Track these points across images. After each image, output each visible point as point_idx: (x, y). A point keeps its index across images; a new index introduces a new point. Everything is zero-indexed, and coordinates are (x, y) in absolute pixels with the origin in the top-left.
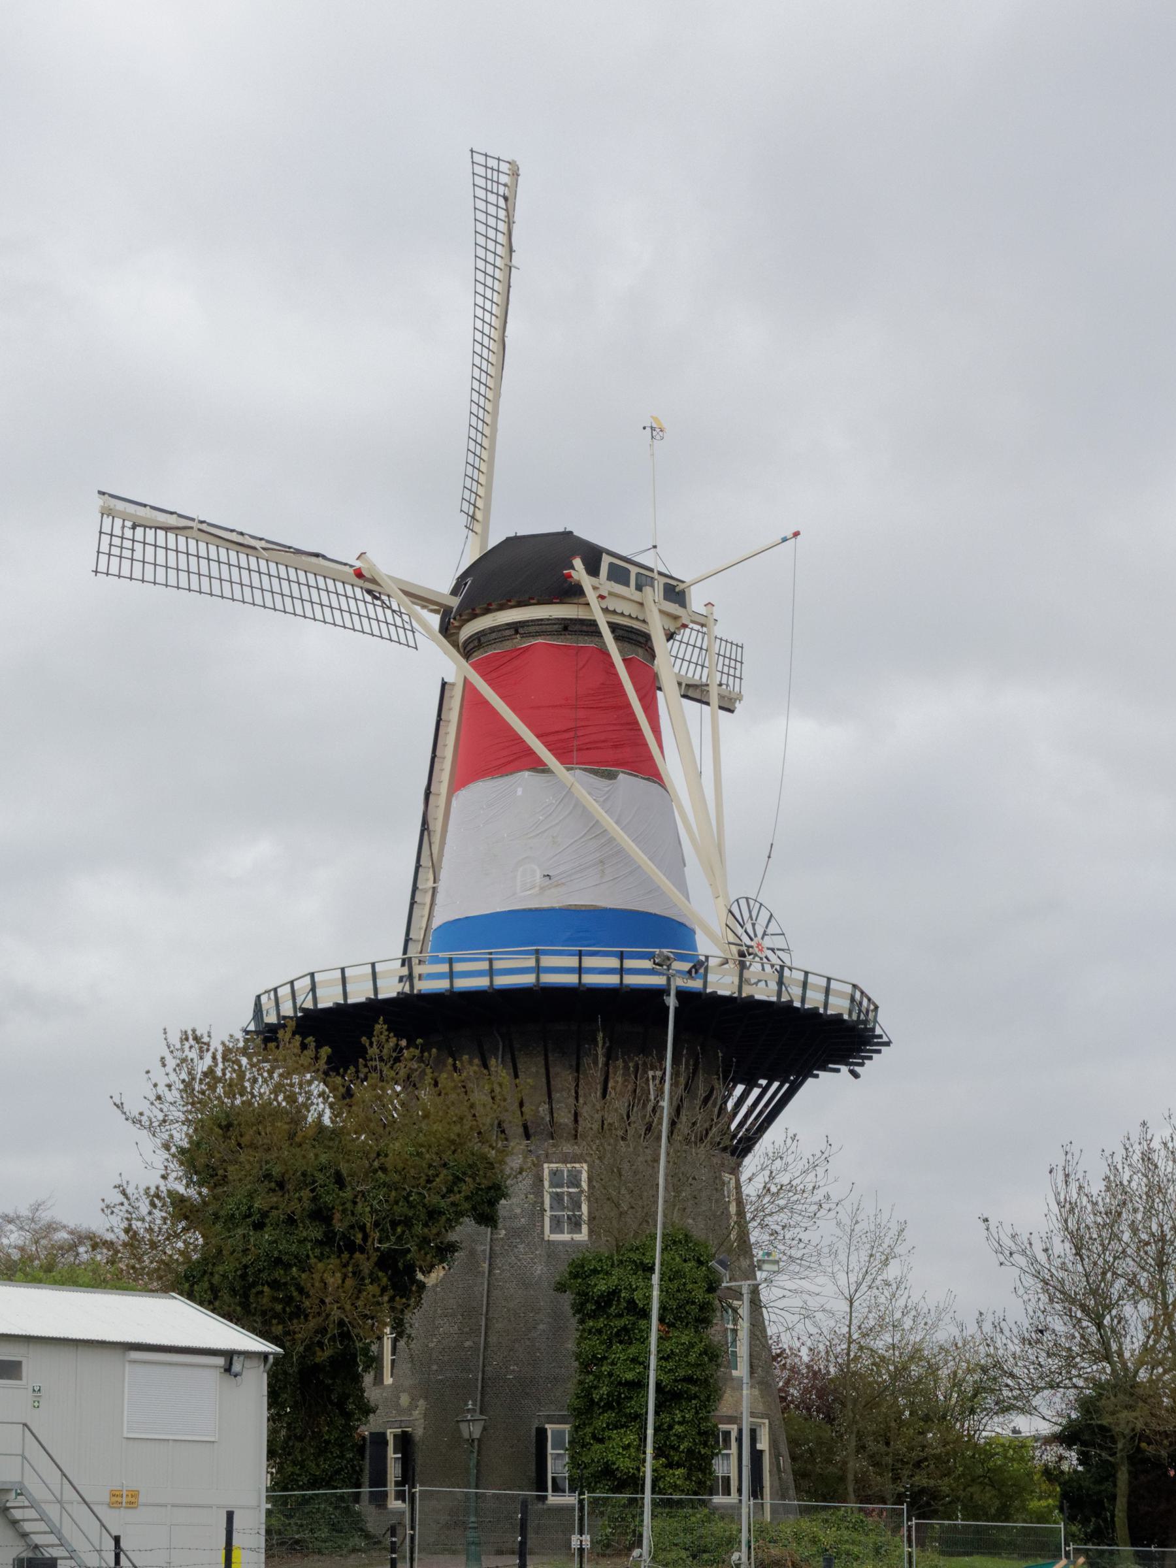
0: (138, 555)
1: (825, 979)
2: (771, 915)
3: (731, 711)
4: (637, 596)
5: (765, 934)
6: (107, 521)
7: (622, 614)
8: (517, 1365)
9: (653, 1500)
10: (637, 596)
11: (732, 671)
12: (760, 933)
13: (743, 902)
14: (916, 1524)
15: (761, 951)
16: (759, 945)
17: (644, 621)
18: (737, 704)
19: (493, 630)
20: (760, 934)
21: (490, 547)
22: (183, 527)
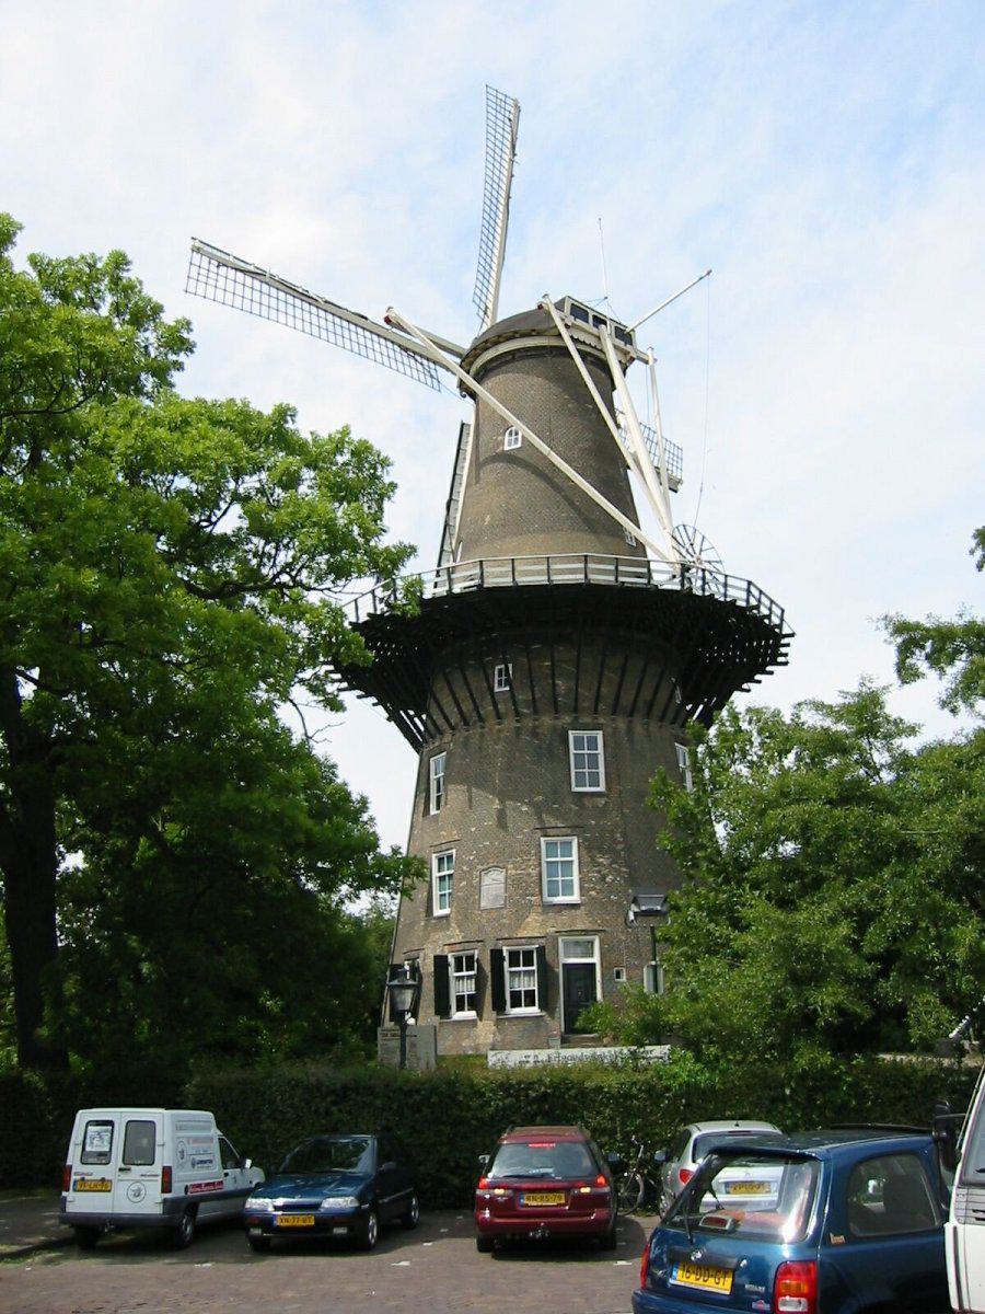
0: (221, 284)
1: (746, 583)
2: (703, 537)
3: (676, 491)
4: (594, 330)
5: (701, 550)
6: (197, 257)
7: (590, 345)
8: (540, 794)
9: (467, 970)
10: (594, 330)
11: (675, 463)
12: (697, 552)
13: (681, 528)
14: (584, 773)
15: (701, 563)
16: (698, 559)
17: (601, 351)
18: (679, 487)
19: (491, 361)
20: (697, 552)
21: (498, 321)
22: (257, 274)
